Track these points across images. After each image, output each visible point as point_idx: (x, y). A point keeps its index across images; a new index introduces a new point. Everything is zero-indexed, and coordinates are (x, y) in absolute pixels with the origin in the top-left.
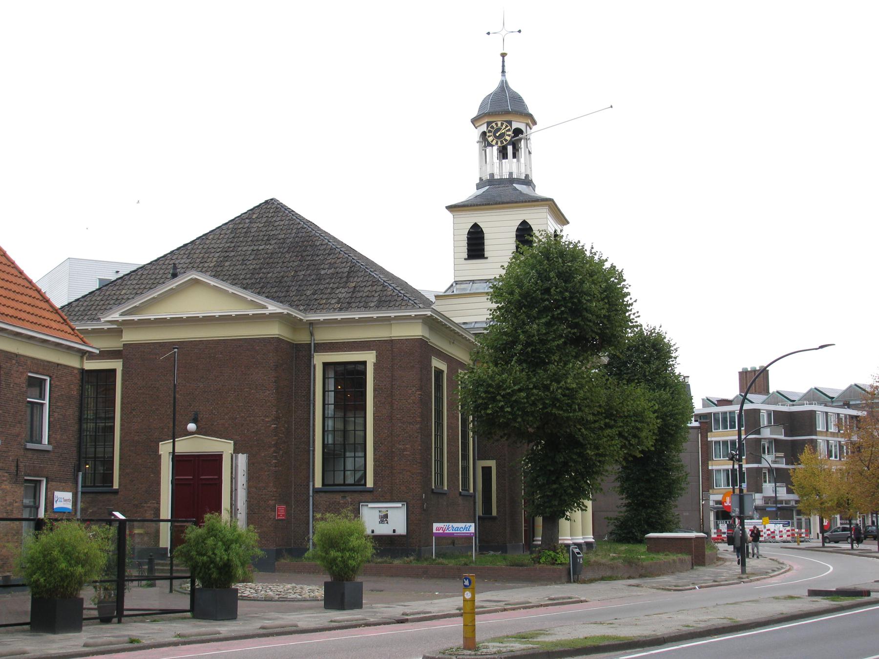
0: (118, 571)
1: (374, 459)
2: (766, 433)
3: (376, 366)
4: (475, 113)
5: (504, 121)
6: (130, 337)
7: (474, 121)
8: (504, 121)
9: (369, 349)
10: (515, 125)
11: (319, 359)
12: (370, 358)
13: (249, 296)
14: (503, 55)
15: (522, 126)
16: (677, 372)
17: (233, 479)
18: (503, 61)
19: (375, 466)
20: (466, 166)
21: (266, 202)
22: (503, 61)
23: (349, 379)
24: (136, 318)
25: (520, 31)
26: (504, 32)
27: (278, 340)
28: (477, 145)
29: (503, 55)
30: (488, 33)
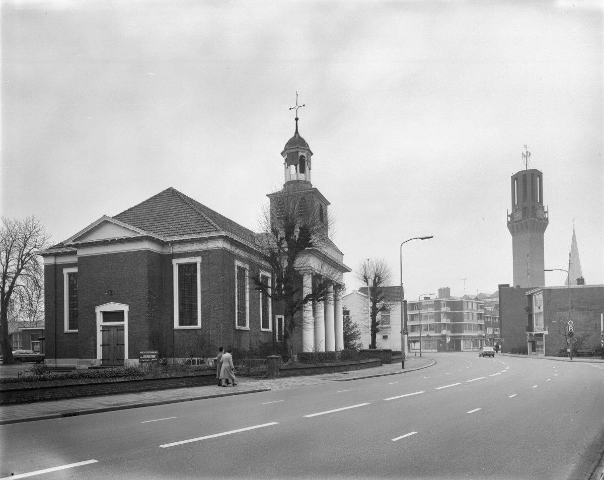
0: (324, 306)
1: (202, 312)
2: (443, 309)
3: (202, 264)
4: (283, 149)
5: (297, 153)
6: (82, 253)
7: (282, 154)
8: (297, 153)
9: (199, 256)
10: (300, 154)
11: (176, 262)
12: (198, 260)
13: (132, 228)
14: (297, 119)
15: (305, 155)
16: (281, 190)
17: (242, 307)
18: (297, 122)
19: (202, 315)
20: (277, 176)
21: (168, 190)
22: (297, 122)
23: (188, 271)
24: (80, 242)
25: (304, 106)
26: (297, 107)
27: (149, 252)
28: (284, 166)
29: (297, 119)
30: (290, 109)
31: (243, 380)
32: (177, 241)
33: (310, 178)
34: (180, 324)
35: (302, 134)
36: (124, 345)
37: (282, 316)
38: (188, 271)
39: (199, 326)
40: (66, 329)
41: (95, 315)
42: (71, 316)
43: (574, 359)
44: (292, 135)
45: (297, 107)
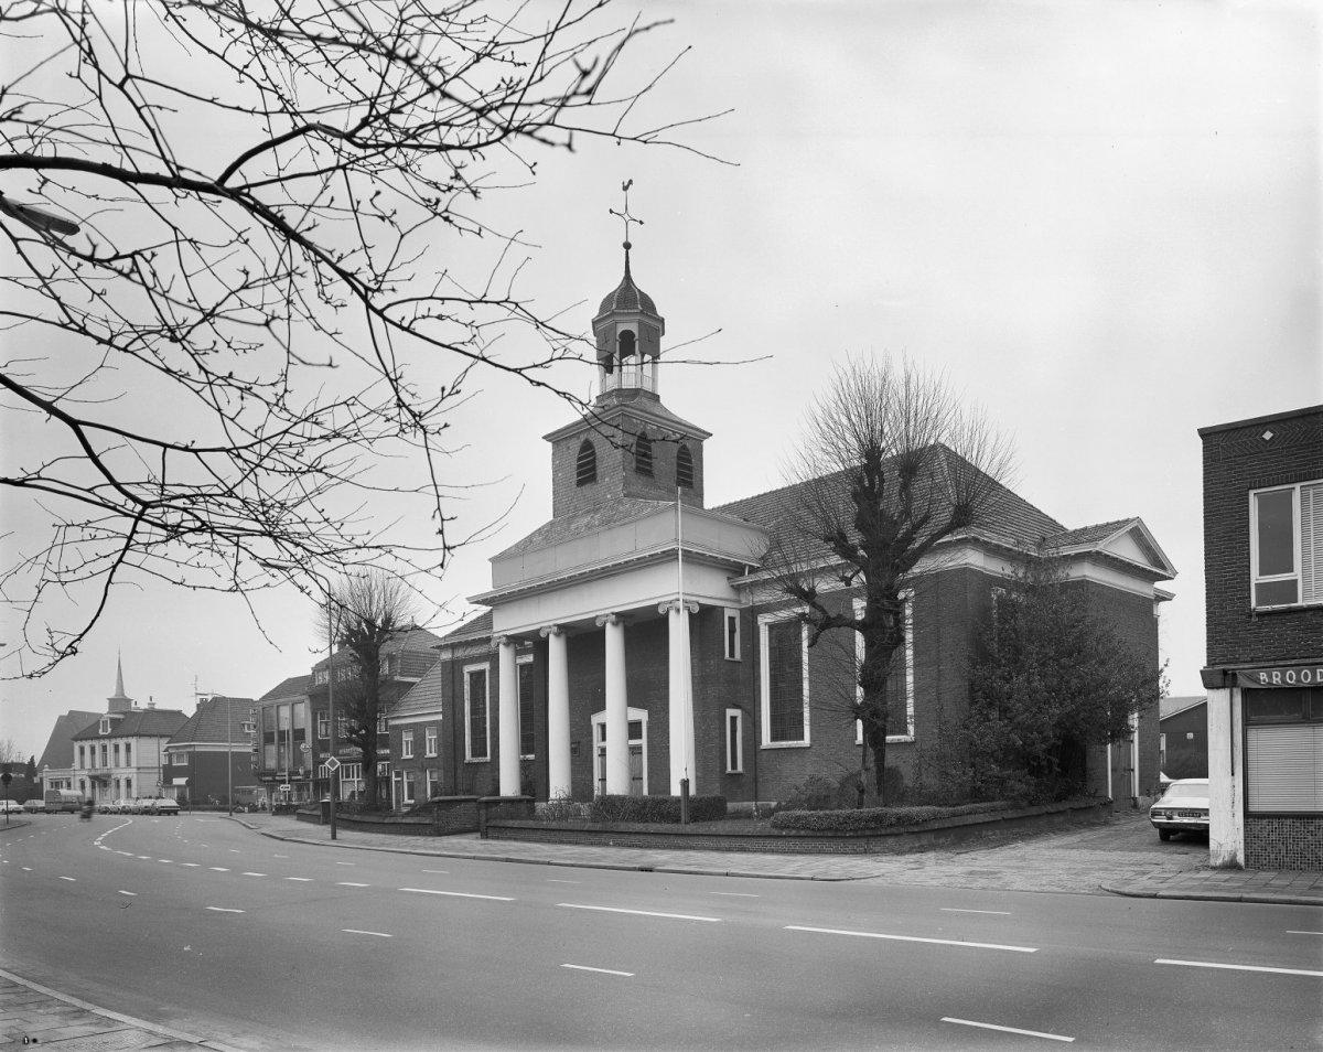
8: (630, 326)
10: (621, 328)
14: (627, 246)
26: (627, 218)
29: (627, 246)
31: (888, 858)
32: (630, 561)
33: (654, 380)
34: (774, 738)
35: (641, 283)
36: (1133, 770)
37: (737, 712)
38: (732, 619)
39: (806, 741)
40: (468, 757)
41: (590, 727)
42: (482, 736)
43: (342, 834)
44: (614, 282)
45: (627, 218)
